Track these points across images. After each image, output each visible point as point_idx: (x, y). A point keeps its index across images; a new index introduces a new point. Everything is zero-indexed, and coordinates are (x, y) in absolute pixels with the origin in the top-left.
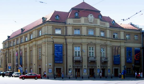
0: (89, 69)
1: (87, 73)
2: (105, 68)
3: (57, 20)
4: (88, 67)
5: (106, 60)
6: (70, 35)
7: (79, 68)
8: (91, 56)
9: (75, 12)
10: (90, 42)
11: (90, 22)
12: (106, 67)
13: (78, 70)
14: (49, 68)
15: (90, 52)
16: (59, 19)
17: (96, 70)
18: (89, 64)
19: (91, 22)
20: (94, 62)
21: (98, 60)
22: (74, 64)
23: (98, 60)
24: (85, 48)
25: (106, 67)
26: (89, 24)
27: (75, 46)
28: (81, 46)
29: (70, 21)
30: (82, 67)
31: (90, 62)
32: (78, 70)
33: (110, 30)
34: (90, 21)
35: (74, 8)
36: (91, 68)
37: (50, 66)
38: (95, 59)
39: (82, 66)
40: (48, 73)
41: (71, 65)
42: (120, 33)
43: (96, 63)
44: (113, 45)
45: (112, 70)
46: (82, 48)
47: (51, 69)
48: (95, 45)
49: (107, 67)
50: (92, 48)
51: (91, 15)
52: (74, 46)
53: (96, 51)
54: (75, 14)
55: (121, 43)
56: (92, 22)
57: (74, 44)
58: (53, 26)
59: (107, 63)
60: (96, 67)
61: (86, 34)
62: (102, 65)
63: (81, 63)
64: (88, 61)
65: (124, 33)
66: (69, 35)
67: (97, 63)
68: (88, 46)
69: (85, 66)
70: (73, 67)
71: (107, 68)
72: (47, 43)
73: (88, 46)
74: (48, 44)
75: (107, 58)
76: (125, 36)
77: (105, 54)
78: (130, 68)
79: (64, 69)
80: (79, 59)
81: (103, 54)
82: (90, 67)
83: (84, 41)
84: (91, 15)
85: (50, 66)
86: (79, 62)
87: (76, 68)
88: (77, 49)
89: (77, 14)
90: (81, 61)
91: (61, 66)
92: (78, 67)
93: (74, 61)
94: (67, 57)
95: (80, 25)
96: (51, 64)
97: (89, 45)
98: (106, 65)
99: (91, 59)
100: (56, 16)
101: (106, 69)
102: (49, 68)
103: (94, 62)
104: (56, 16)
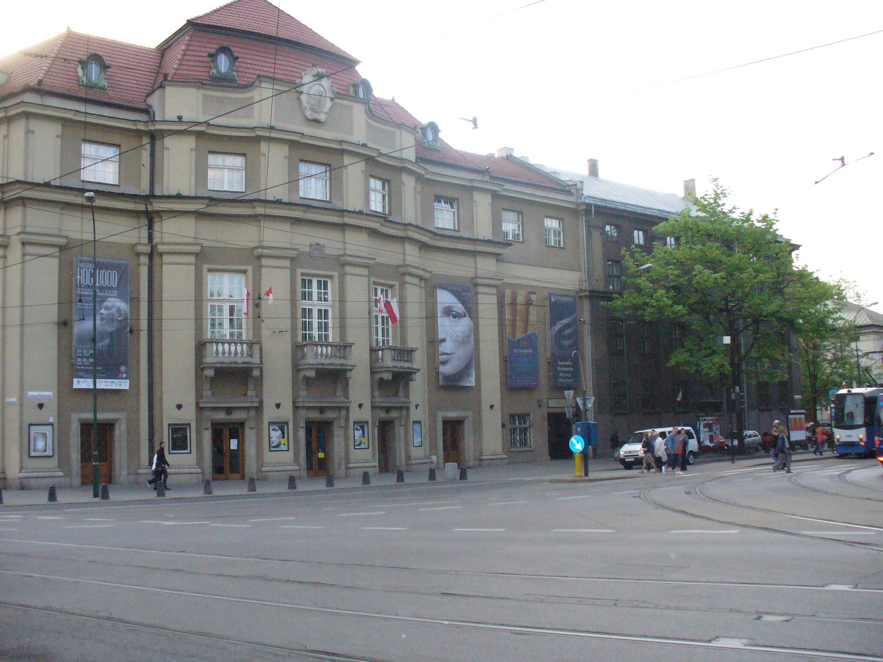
0: (303, 424)
1: (291, 454)
2: (329, 415)
3: (91, 86)
4: (296, 408)
5: (406, 365)
6: (179, 197)
7: (237, 416)
8: (311, 336)
9: (217, 46)
10: (307, 250)
11: (309, 114)
12: (400, 408)
13: (318, 434)
14: (30, 425)
15: (310, 310)
16: (105, 83)
17: (346, 428)
18: (303, 393)
19: (315, 116)
20: (334, 377)
21: (359, 359)
22: (207, 393)
23: (359, 359)
24: (277, 280)
25: (400, 408)
26: (307, 130)
27: (211, 266)
28: (250, 268)
29: (180, 104)
30: (259, 409)
31: (308, 381)
32: (318, 434)
33: (419, 178)
34: (313, 110)
35: (216, 21)
36: (314, 415)
37: (41, 406)
38: (344, 358)
39: (261, 403)
40: (27, 461)
41: (189, 399)
42: (472, 201)
43: (347, 380)
44: (435, 271)
45: (432, 428)
46: (257, 282)
47: (50, 428)
48: (341, 263)
49: (408, 408)
50: (319, 282)
51: (319, 77)
52: (205, 267)
53: (342, 301)
54: (213, 56)
55: (478, 258)
56: (322, 117)
57: (205, 258)
58: (153, 121)
59: (259, 381)
60: (347, 409)
61: (281, 193)
62: (377, 393)
63: (251, 386)
64: (296, 369)
65: (492, 205)
66: (174, 193)
67: (350, 381)
68: (299, 271)
69: (278, 406)
70: (200, 409)
71: (408, 415)
72: (24, 244)
73: (299, 271)
74: (30, 249)
75: (344, 347)
76: (497, 223)
77: (248, 329)
78: (528, 415)
79: (132, 431)
80: (240, 360)
81: (315, 322)
82: (309, 408)
83: (275, 235)
84: (315, 70)
85: (41, 406)
86: (238, 377)
87: (221, 416)
88: (229, 287)
89: (223, 62)
90: (256, 373)
91: (113, 410)
92: (229, 410)
93: (210, 373)
94: (156, 352)
95: (253, 129)
96: (50, 393)
97: (301, 267)
98: (401, 394)
99: (319, 356)
100: (85, 58)
101: (403, 423)
102: (30, 425)
103: (334, 377)
104: (83, 64)
